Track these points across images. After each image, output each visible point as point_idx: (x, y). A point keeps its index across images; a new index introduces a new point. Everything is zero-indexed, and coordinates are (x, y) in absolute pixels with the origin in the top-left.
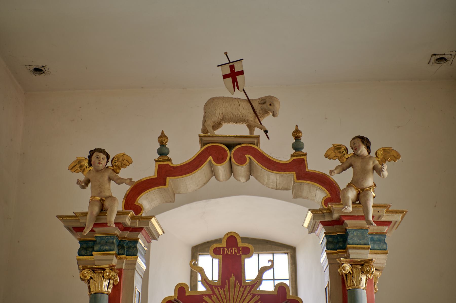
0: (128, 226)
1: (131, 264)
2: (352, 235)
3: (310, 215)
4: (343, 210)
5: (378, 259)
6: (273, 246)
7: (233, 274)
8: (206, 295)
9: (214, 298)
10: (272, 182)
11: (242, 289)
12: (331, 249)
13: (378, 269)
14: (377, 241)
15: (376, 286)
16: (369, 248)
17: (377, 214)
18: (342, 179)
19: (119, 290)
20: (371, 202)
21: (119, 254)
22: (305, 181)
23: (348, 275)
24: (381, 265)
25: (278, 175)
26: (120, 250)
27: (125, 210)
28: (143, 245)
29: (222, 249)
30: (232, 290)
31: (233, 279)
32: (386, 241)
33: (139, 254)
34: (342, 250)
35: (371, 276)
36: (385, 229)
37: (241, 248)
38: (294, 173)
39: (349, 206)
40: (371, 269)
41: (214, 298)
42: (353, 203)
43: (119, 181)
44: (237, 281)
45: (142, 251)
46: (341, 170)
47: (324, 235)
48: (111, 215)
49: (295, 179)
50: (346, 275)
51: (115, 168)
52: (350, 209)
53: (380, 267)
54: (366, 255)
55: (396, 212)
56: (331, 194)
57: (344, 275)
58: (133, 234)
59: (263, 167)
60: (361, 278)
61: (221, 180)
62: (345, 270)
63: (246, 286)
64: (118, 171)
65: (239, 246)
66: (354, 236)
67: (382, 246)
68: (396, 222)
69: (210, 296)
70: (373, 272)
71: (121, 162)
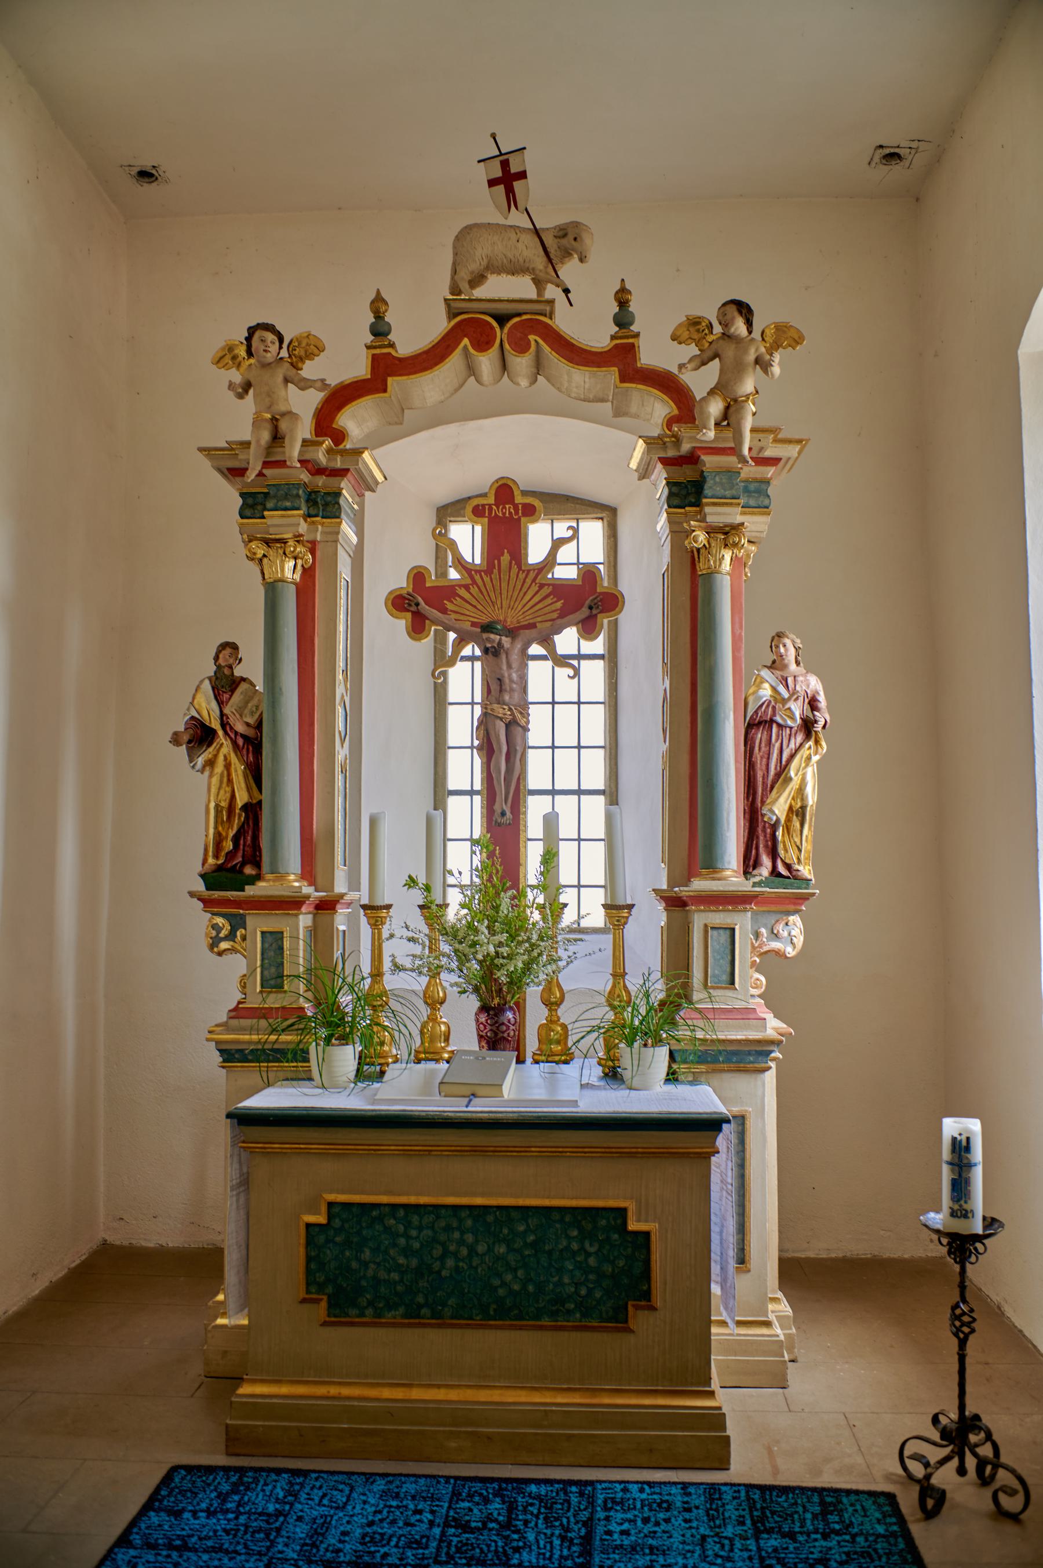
3: (641, 445)
5: (754, 524)
8: (460, 586)
9: (474, 590)
11: (522, 576)
18: (700, 381)
20: (748, 423)
21: (310, 516)
23: (702, 551)
24: (758, 534)
27: (317, 436)
28: (350, 500)
30: (504, 577)
31: (506, 558)
32: (769, 492)
33: (343, 516)
34: (694, 509)
36: (770, 471)
38: (616, 369)
40: (740, 540)
41: (474, 590)
42: (717, 424)
43: (302, 384)
47: (664, 482)
48: (292, 446)
49: (618, 380)
50: (698, 550)
52: (711, 434)
54: (733, 515)
55: (789, 441)
56: (679, 408)
58: (332, 481)
61: (486, 383)
62: (696, 542)
63: (529, 571)
64: (300, 365)
66: (715, 483)
71: (304, 349)
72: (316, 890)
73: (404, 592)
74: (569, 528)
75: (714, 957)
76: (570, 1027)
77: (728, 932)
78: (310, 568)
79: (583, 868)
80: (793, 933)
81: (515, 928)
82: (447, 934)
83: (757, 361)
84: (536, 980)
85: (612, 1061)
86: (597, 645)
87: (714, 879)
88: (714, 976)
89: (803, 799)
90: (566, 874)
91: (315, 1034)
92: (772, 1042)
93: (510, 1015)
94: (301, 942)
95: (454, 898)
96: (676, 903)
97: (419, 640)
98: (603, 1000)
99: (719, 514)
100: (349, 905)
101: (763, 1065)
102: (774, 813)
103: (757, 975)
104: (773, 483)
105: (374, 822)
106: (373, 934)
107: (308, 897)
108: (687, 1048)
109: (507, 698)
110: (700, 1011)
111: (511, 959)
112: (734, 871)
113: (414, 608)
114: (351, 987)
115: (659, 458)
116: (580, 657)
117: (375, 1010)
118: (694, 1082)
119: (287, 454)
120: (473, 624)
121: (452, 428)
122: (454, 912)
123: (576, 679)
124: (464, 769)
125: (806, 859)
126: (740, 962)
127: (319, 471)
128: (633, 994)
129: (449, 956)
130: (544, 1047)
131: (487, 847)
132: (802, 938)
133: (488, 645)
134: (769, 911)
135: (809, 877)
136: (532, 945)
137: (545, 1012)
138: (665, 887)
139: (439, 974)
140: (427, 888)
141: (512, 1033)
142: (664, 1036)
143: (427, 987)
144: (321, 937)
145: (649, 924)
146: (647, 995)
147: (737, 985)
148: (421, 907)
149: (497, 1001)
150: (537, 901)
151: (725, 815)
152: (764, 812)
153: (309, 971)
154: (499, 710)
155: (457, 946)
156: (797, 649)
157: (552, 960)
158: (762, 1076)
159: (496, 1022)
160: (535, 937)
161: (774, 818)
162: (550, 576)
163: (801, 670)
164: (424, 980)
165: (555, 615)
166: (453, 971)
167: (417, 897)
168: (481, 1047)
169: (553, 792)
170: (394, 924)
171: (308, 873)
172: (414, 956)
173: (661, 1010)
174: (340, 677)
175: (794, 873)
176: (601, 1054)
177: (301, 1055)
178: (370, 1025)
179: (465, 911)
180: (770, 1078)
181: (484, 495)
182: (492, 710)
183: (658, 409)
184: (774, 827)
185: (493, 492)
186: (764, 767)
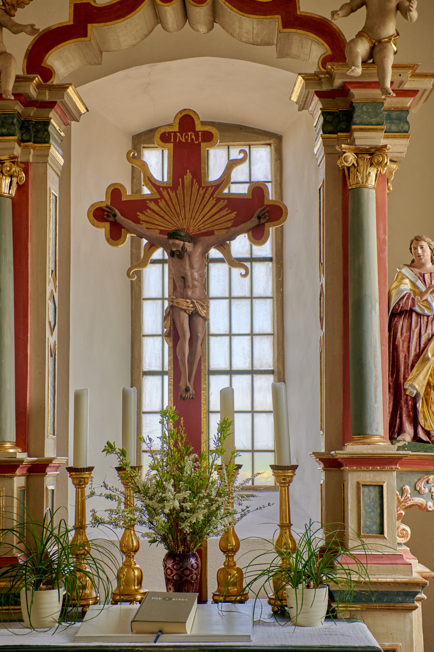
0: (33, 99)
1: (41, 156)
2: (360, 111)
4: (348, 73)
5: (396, 146)
6: (249, 134)
7: (188, 171)
8: (151, 200)
9: (162, 204)
10: (247, 33)
11: (202, 192)
13: (394, 160)
14: (396, 119)
15: (389, 184)
16: (383, 130)
17: (398, 79)
18: (349, 26)
19: (26, 193)
20: (390, 61)
21: (23, 141)
22: (294, 30)
23: (352, 169)
24: (398, 155)
25: (255, 20)
26: (24, 135)
27: (28, 73)
28: (58, 128)
29: (172, 134)
30: (187, 192)
31: (188, 177)
32: (408, 119)
33: (51, 141)
34: (345, 134)
35: (383, 170)
36: (409, 102)
37: (200, 133)
38: (279, 16)
39: (358, 67)
40: (383, 160)
41: (162, 204)
42: (364, 62)
43: (15, 29)
44: (195, 180)
45: (57, 138)
46: (349, 11)
47: (320, 112)
48: (7, 82)
49: (281, 26)
50: (349, 168)
51: (8, 7)
52: (359, 71)
53: (397, 157)
54: (377, 138)
55: (425, 76)
56: (332, 49)
57: (345, 168)
58: (42, 111)
59: (233, 8)
60: (370, 173)
61: (171, 30)
62: (346, 162)
63: (207, 188)
64: (12, 12)
65: (197, 130)
66: (363, 112)
67: (402, 127)
68: (425, 90)
69: (156, 201)
70: (386, 164)
72: (29, 456)
73: (103, 205)
74: (240, 152)
75: (365, 510)
76: (244, 571)
77: (377, 489)
78: (23, 185)
79: (254, 433)
81: (196, 487)
82: (139, 492)
83: (398, 7)
84: (215, 531)
85: (280, 600)
86: (266, 249)
87: (364, 444)
88: (366, 526)
90: (241, 440)
91: (26, 580)
92: (417, 584)
93: (193, 561)
94: (15, 500)
95: (147, 461)
97: (117, 245)
98: (271, 547)
99: (366, 138)
100: (57, 468)
101: (410, 605)
102: (414, 388)
103: (403, 526)
104: (413, 111)
105: (78, 397)
106: (77, 493)
107: (21, 461)
109: (190, 293)
110: (354, 557)
111: (194, 513)
113: (112, 219)
114: (57, 539)
115: (315, 92)
116: (252, 260)
117: (78, 558)
118: (351, 620)
119: (3, 89)
120: (162, 232)
121: (144, 69)
122: (146, 474)
123: (249, 277)
124: (155, 353)
126: (388, 514)
127: (28, 102)
128: (297, 542)
129: (141, 511)
130: (222, 588)
131: (173, 418)
133: (174, 249)
134: (412, 472)
136: (211, 500)
137: (223, 558)
138: (323, 450)
139: (133, 526)
140: (123, 453)
141: (195, 577)
142: (324, 578)
143: (123, 537)
144: (33, 495)
145: (311, 480)
146: (309, 543)
147: (386, 535)
148: (119, 469)
149: (181, 549)
150: (215, 463)
151: (373, 390)
152: (406, 387)
153: (21, 524)
154: (183, 303)
155: (148, 501)
157: (228, 514)
158: (410, 614)
159: (181, 567)
160: (214, 493)
161: (415, 392)
162: (226, 191)
164: (120, 532)
165: (230, 224)
166: (144, 523)
167: (114, 460)
168: (168, 589)
169: (231, 372)
170: (95, 483)
171: (22, 442)
172: (111, 511)
173: (321, 556)
174: (49, 276)
176: (271, 594)
177: (15, 600)
178: (73, 571)
179: (155, 472)
180: (417, 616)
181: (170, 125)
182: (178, 303)
183: (312, 51)
184: (415, 399)
185: (177, 121)
186: (406, 350)
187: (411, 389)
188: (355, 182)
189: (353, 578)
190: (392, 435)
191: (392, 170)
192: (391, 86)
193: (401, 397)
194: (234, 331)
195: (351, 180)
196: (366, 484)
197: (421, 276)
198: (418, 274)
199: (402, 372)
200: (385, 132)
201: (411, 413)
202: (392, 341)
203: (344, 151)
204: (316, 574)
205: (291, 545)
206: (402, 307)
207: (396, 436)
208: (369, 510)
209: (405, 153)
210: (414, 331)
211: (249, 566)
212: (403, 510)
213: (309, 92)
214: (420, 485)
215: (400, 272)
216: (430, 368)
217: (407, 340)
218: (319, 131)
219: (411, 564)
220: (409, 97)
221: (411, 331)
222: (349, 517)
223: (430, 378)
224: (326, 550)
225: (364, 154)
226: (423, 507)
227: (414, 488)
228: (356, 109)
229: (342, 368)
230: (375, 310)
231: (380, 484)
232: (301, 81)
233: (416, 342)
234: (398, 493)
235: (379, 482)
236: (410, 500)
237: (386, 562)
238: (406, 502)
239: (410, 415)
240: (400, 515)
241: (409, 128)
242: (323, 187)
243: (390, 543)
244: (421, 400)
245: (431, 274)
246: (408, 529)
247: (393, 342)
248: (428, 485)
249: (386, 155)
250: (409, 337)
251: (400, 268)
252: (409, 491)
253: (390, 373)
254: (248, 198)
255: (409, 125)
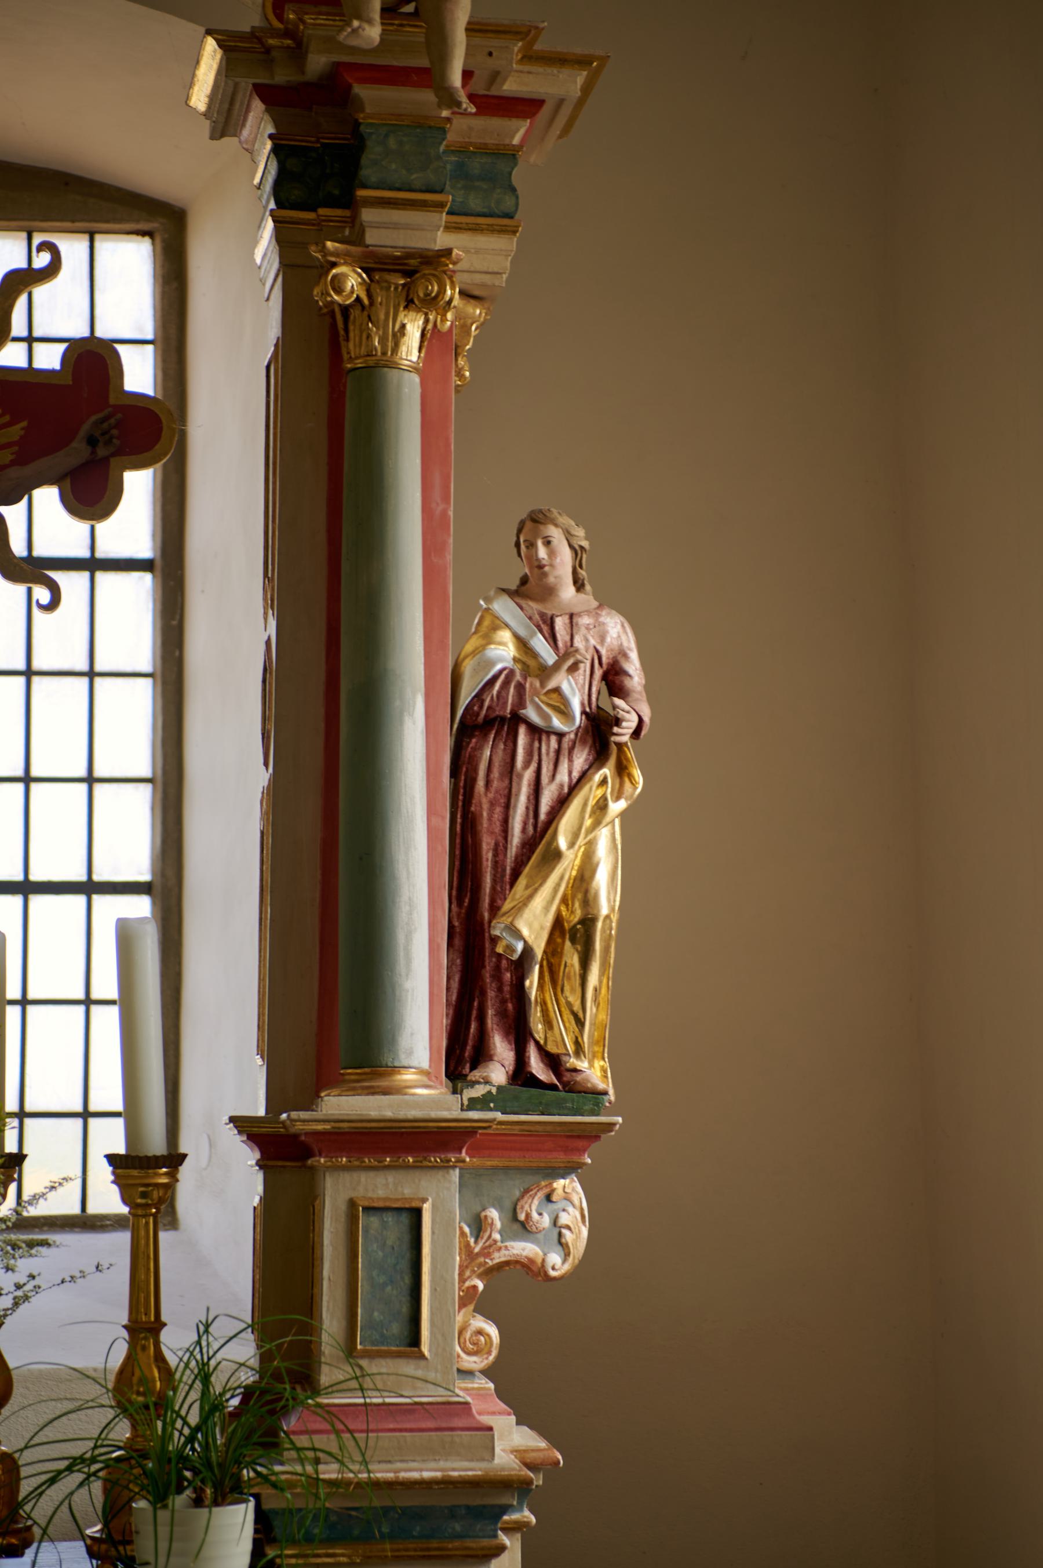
3: (211, 55)
4: (341, 37)
5: (478, 255)
12: (294, 207)
13: (476, 293)
15: (461, 362)
23: (355, 313)
24: (487, 279)
34: (339, 212)
35: (444, 319)
36: (518, 131)
39: (370, 22)
40: (442, 291)
47: (269, 145)
50: (345, 310)
52: (373, 33)
53: (483, 285)
55: (561, 60)
60: (403, 326)
62: (339, 291)
68: (561, 102)
80: (564, 1219)
87: (373, 1091)
88: (370, 1325)
89: (588, 901)
96: (280, 1148)
99: (396, 226)
101: (485, 1542)
103: (480, 1323)
108: (300, 1504)
112: (421, 1072)
125: (593, 1043)
132: (585, 1232)
134: (506, 1169)
135: (601, 1086)
145: (222, 1194)
152: (496, 932)
156: (577, 552)
161: (520, 947)
163: (587, 600)
175: (567, 1077)
184: (521, 965)
186: (497, 828)
187: (508, 938)
188: (363, 351)
189: (324, 1473)
190: (456, 1068)
191: (470, 321)
192: (464, 85)
193: (483, 961)
194: (35, 772)
195: (351, 345)
196: (376, 1205)
197: (544, 622)
198: (537, 617)
199: (488, 890)
200: (448, 213)
201: (510, 1006)
202: (460, 804)
203: (333, 259)
204: (220, 1465)
205: (158, 1384)
206: (489, 708)
207: (467, 1069)
208: (382, 1279)
209: (505, 276)
210: (520, 777)
211: (26, 1447)
212: (480, 1277)
213: (236, 85)
214: (527, 1207)
215: (487, 610)
216: (562, 878)
217: (502, 801)
218: (268, 202)
219: (491, 1429)
220: (517, 117)
221: (514, 777)
222: (325, 1298)
223: (563, 908)
224: (254, 1393)
225: (389, 271)
226: (535, 1269)
227: (510, 1215)
228: (369, 143)
229: (319, 877)
230: (412, 715)
231: (414, 1204)
232: (215, 51)
233: (527, 808)
234: (467, 1230)
235: (412, 1199)
236: (499, 1249)
237: (423, 1425)
238: (488, 1255)
239: (506, 1010)
240: (471, 1291)
241: (517, 205)
242: (277, 362)
243: (436, 1371)
244: (537, 968)
245: (571, 616)
246: (493, 1331)
247: (463, 806)
248: (551, 1206)
249: (451, 278)
250: (506, 791)
251: (488, 600)
252: (498, 1224)
253: (454, 893)
254: (62, 382)
255: (517, 197)
